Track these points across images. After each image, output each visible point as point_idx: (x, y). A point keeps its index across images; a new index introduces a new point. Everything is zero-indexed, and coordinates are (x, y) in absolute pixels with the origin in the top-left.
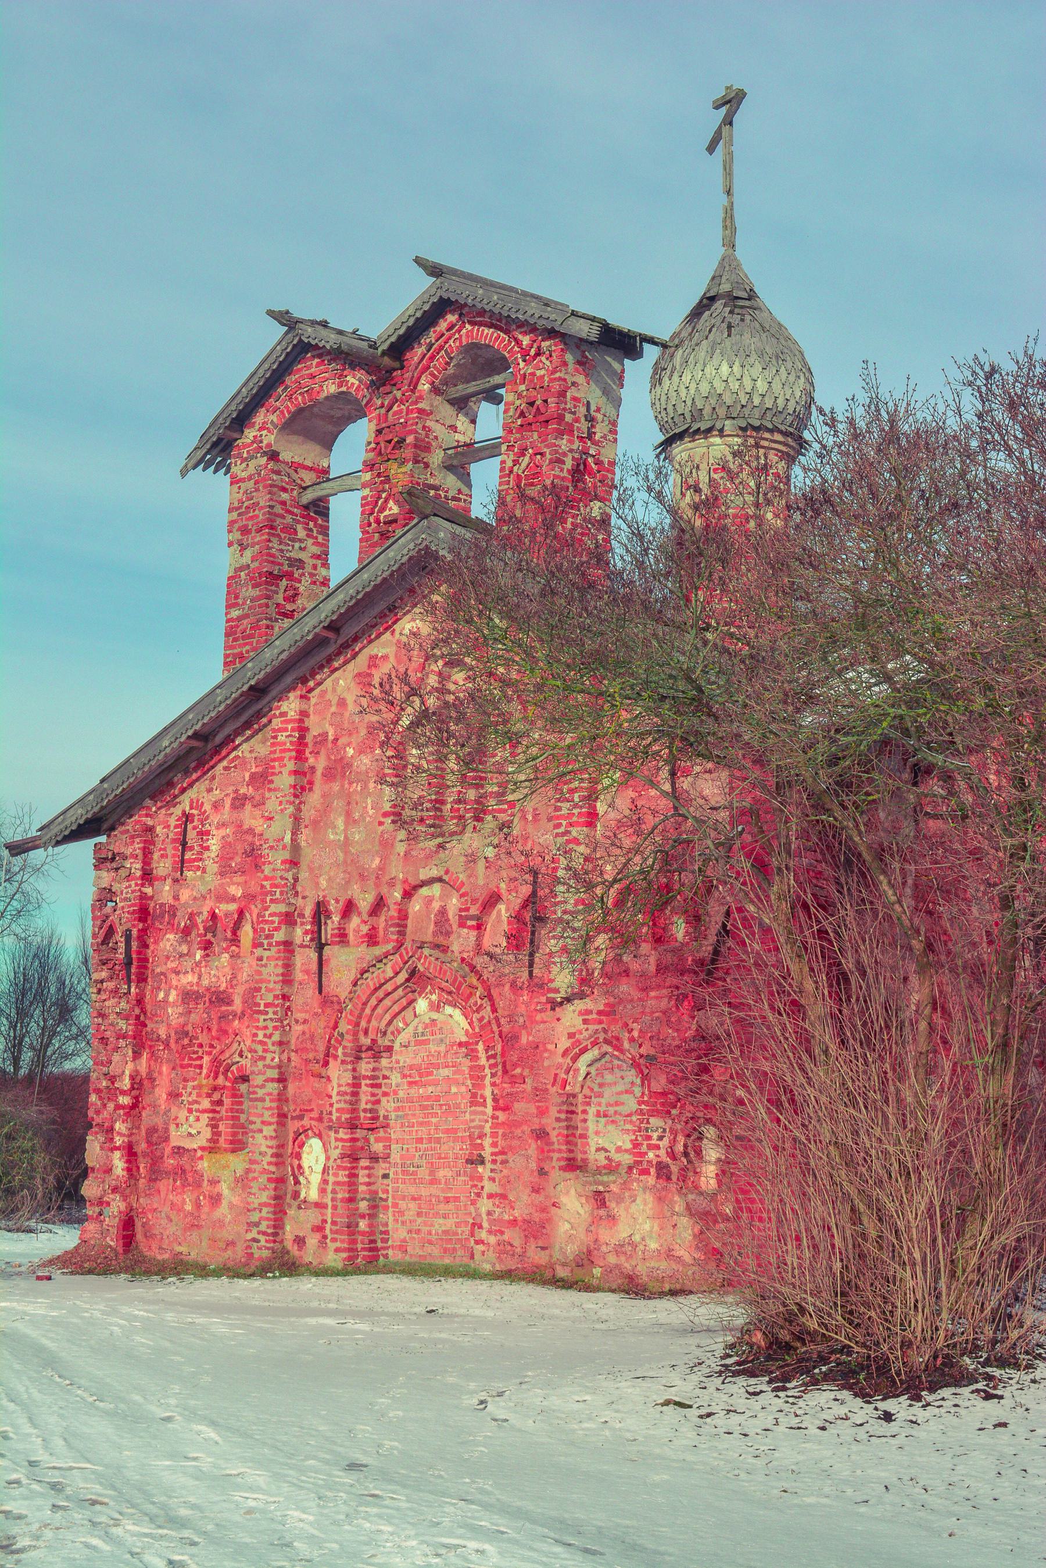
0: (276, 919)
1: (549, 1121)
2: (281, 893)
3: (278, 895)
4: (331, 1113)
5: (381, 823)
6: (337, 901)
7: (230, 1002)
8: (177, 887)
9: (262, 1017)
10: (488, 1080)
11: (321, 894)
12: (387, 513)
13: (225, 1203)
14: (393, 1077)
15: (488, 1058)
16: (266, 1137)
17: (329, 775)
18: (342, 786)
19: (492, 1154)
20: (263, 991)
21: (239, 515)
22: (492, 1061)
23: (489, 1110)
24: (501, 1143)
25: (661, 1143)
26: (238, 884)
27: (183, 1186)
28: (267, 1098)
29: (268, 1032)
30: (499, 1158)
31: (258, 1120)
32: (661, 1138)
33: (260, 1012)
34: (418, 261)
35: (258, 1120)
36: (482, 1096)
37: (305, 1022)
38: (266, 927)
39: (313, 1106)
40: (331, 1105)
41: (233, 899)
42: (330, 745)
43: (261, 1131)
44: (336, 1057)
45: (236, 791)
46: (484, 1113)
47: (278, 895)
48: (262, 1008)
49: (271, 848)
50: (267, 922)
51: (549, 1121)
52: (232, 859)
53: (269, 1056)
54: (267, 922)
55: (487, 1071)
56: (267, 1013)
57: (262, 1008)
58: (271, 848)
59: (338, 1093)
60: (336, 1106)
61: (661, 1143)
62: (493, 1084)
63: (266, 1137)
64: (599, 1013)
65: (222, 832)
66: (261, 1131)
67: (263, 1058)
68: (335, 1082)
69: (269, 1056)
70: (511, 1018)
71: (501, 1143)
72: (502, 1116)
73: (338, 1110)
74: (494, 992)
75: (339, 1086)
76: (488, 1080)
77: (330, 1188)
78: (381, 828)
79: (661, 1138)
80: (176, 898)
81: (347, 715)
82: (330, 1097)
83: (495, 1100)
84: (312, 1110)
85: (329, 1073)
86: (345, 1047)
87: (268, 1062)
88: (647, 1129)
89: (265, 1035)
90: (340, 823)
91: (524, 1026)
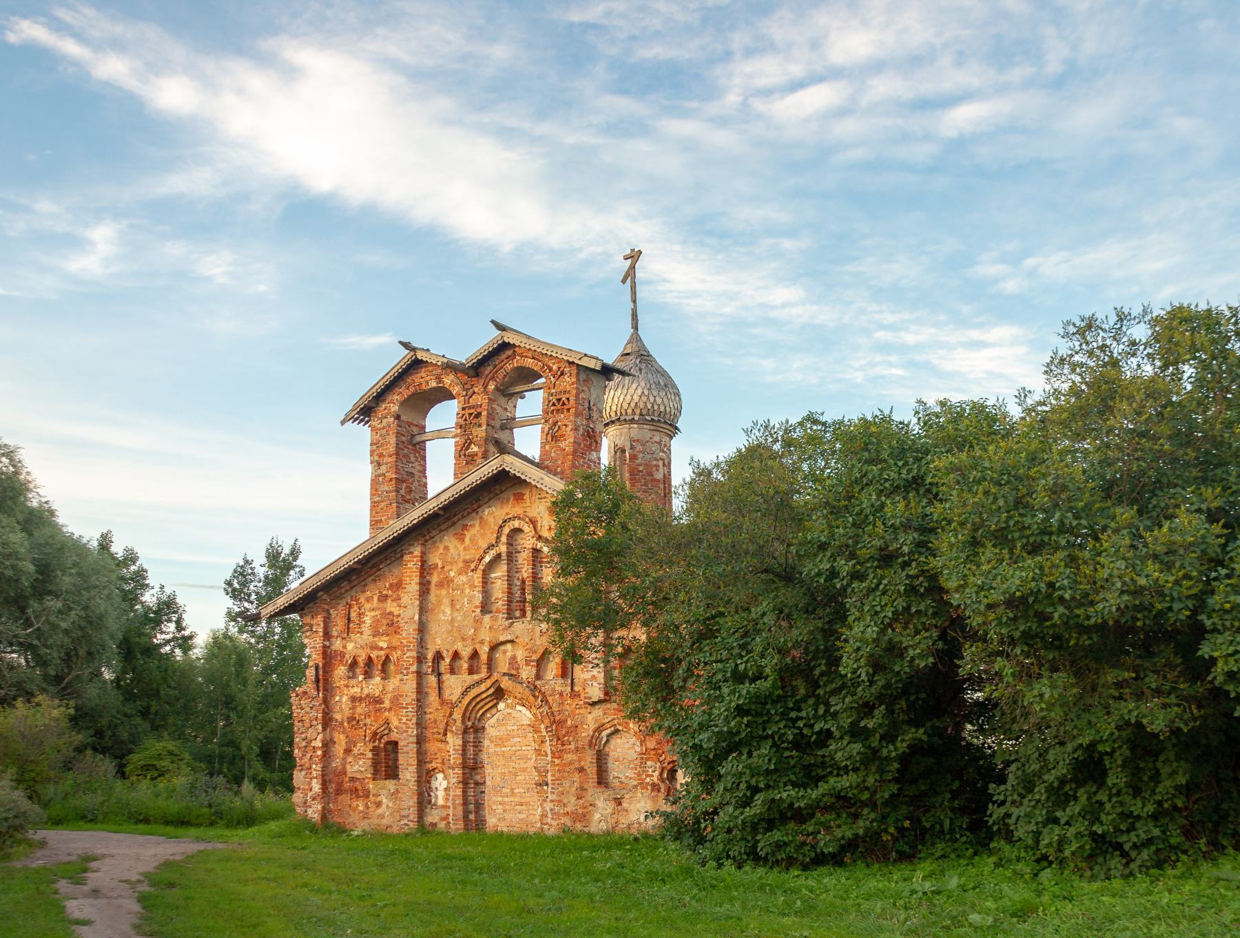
6: (448, 651)
8: (344, 642)
13: (384, 806)
23: (549, 758)
32: (654, 771)
34: (493, 322)
41: (382, 649)
53: (410, 730)
55: (547, 738)
62: (551, 745)
65: (373, 614)
68: (451, 744)
72: (557, 761)
77: (451, 798)
80: (345, 647)
83: (552, 752)
87: (409, 733)
90: (448, 610)
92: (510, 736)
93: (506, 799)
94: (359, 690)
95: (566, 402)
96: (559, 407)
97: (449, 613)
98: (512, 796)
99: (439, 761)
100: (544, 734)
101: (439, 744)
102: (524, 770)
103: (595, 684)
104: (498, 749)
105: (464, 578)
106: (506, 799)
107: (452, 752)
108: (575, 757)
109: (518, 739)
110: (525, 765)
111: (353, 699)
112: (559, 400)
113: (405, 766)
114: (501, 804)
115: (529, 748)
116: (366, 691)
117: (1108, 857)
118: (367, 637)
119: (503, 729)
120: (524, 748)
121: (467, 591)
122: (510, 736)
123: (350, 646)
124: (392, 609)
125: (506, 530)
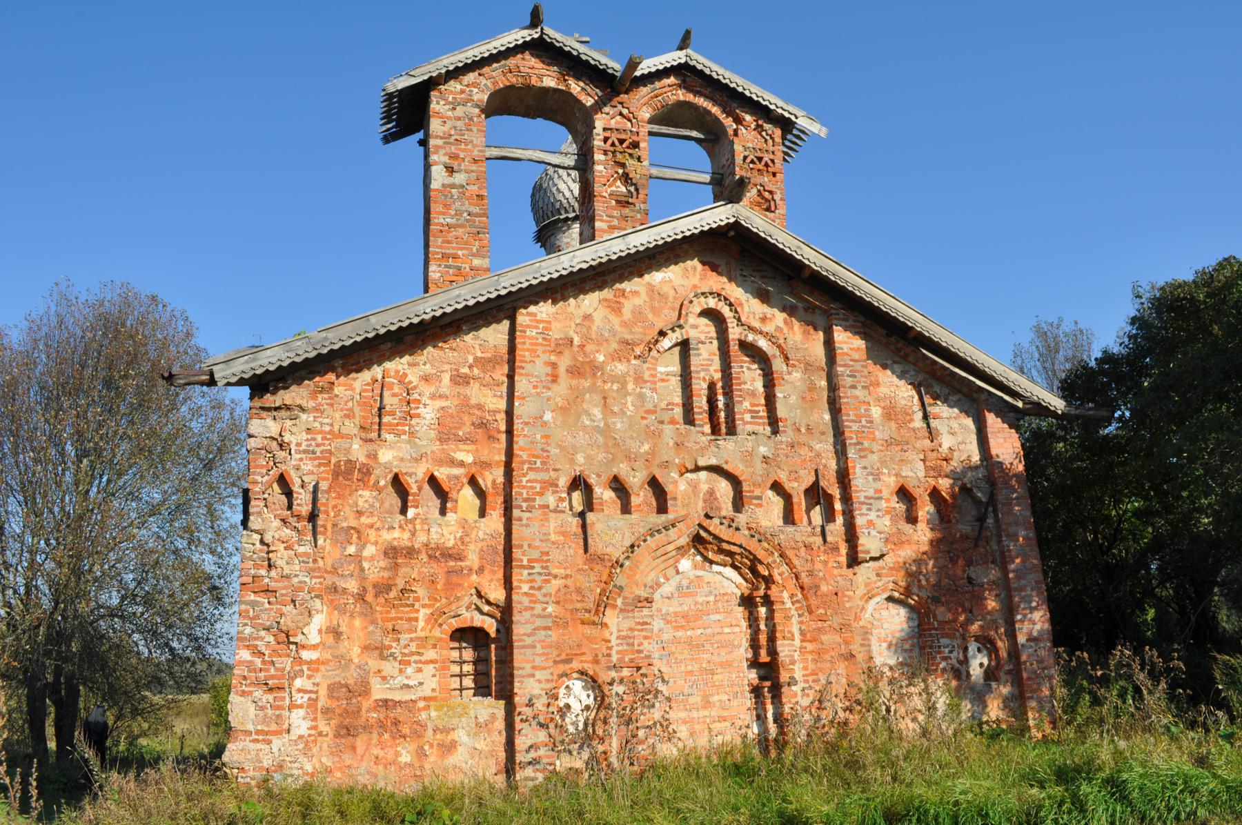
0: (538, 486)
1: (855, 647)
2: (542, 463)
3: (538, 464)
4: (609, 655)
5: (643, 418)
6: (599, 476)
7: (460, 557)
8: (371, 447)
9: (525, 572)
10: (795, 620)
11: (578, 469)
12: (613, 188)
14: (655, 623)
15: (793, 603)
16: (540, 681)
17: (575, 371)
18: (594, 384)
19: (804, 676)
20: (526, 547)
21: (445, 143)
22: (798, 605)
23: (797, 642)
24: (811, 666)
25: (952, 655)
26: (468, 451)
27: (906, 651)
28: (538, 646)
29: (536, 585)
30: (810, 678)
31: (528, 666)
32: (951, 652)
33: (524, 567)
35: (528, 666)
36: (790, 632)
37: (566, 577)
38: (524, 491)
39: (584, 650)
40: (610, 648)
41: (462, 464)
42: (575, 349)
43: (533, 676)
44: (614, 606)
45: (457, 370)
46: (793, 645)
47: (538, 464)
48: (525, 563)
49: (527, 423)
50: (524, 487)
51: (855, 647)
52: (459, 428)
54: (524, 487)
55: (793, 612)
56: (533, 568)
57: (525, 563)
58: (527, 423)
59: (618, 638)
60: (615, 649)
61: (952, 655)
62: (801, 623)
63: (540, 681)
64: (891, 569)
65: (439, 403)
66: (533, 676)
67: (533, 609)
68: (614, 629)
69: (538, 607)
70: (811, 573)
71: (811, 666)
72: (810, 646)
73: (618, 652)
74: (790, 553)
75: (619, 631)
76: (795, 620)
78: (645, 422)
79: (951, 652)
80: (373, 456)
81: (594, 328)
82: (609, 641)
83: (802, 633)
84: (584, 654)
85: (606, 620)
86: (625, 598)
88: (939, 647)
89: (532, 588)
90: (597, 412)
91: (824, 579)
92: (701, 613)
93: (695, 714)
94: (406, 535)
95: (771, 164)
96: (761, 166)
97: (600, 416)
98: (705, 707)
99: (589, 657)
100: (789, 605)
101: (588, 630)
102: (727, 665)
103: (874, 533)
104: (679, 634)
105: (620, 368)
106: (695, 714)
107: (614, 641)
108: (837, 639)
109: (717, 617)
110: (730, 658)
111: (392, 552)
112: (760, 159)
113: (528, 670)
114: (685, 722)
115: (737, 629)
116: (422, 538)
117: (683, 763)
118: (427, 440)
119: (689, 601)
120: (727, 630)
121: (630, 386)
122: (701, 613)
123: (385, 456)
124: (482, 400)
125: (726, 312)
